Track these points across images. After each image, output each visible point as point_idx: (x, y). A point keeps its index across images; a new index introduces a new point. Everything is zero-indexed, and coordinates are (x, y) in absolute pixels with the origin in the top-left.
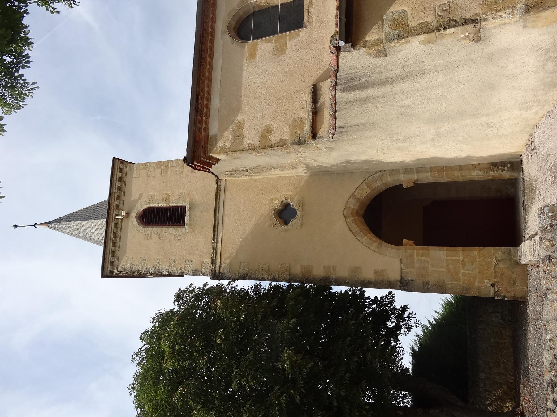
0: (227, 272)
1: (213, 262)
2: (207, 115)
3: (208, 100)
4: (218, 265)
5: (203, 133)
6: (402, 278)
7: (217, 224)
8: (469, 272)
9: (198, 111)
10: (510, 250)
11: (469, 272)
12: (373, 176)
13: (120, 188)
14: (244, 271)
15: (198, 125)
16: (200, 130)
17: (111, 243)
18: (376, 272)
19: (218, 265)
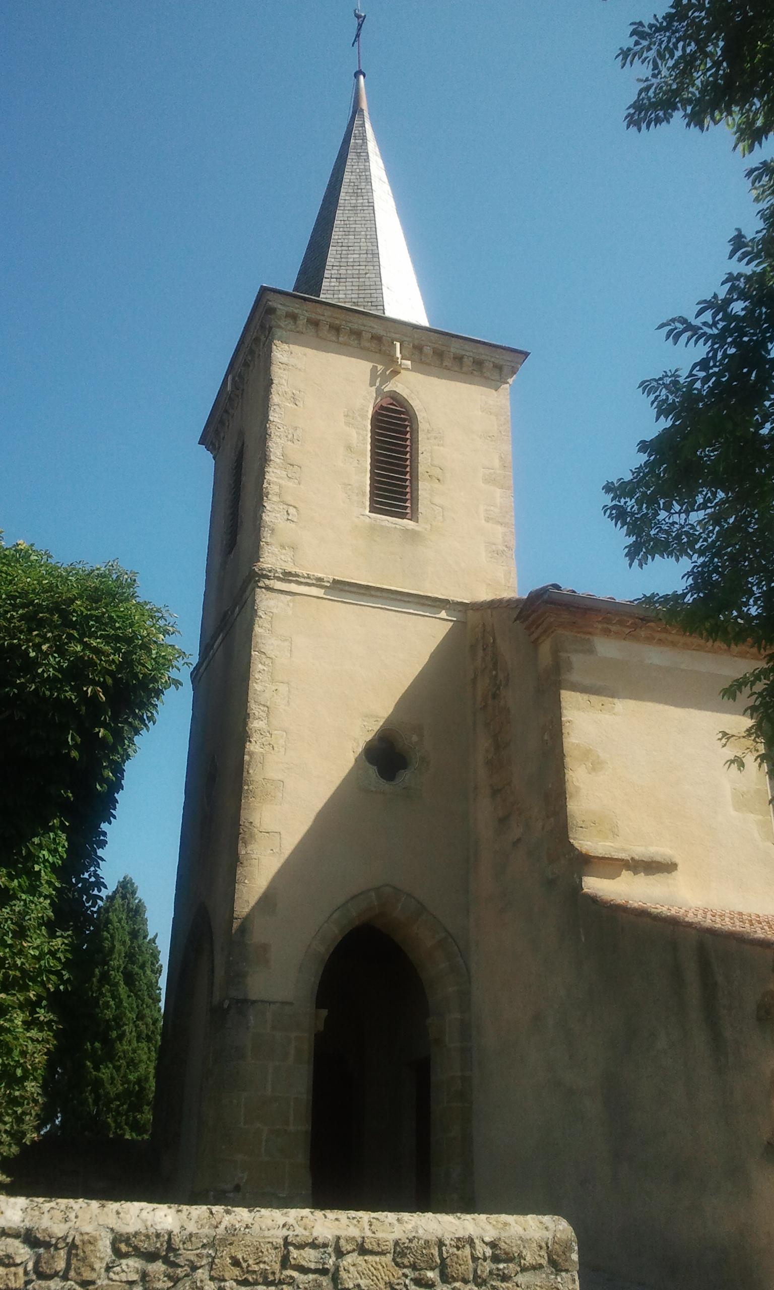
0: (268, 607)
1: (287, 576)
2: (631, 636)
3: (661, 642)
4: (278, 585)
5: (600, 626)
6: (253, 1002)
7: (373, 593)
8: (264, 1144)
9: (642, 619)
10: (387, 1215)
11: (264, 1144)
12: (459, 955)
13: (459, 359)
14: (271, 648)
15: (617, 619)
16: (607, 621)
17: (337, 322)
18: (265, 948)
19: (278, 585)
